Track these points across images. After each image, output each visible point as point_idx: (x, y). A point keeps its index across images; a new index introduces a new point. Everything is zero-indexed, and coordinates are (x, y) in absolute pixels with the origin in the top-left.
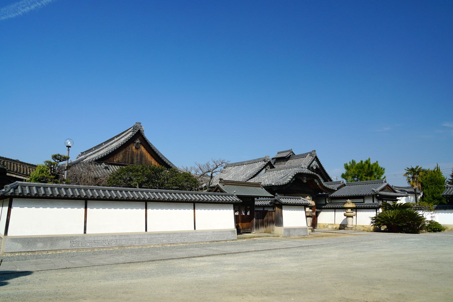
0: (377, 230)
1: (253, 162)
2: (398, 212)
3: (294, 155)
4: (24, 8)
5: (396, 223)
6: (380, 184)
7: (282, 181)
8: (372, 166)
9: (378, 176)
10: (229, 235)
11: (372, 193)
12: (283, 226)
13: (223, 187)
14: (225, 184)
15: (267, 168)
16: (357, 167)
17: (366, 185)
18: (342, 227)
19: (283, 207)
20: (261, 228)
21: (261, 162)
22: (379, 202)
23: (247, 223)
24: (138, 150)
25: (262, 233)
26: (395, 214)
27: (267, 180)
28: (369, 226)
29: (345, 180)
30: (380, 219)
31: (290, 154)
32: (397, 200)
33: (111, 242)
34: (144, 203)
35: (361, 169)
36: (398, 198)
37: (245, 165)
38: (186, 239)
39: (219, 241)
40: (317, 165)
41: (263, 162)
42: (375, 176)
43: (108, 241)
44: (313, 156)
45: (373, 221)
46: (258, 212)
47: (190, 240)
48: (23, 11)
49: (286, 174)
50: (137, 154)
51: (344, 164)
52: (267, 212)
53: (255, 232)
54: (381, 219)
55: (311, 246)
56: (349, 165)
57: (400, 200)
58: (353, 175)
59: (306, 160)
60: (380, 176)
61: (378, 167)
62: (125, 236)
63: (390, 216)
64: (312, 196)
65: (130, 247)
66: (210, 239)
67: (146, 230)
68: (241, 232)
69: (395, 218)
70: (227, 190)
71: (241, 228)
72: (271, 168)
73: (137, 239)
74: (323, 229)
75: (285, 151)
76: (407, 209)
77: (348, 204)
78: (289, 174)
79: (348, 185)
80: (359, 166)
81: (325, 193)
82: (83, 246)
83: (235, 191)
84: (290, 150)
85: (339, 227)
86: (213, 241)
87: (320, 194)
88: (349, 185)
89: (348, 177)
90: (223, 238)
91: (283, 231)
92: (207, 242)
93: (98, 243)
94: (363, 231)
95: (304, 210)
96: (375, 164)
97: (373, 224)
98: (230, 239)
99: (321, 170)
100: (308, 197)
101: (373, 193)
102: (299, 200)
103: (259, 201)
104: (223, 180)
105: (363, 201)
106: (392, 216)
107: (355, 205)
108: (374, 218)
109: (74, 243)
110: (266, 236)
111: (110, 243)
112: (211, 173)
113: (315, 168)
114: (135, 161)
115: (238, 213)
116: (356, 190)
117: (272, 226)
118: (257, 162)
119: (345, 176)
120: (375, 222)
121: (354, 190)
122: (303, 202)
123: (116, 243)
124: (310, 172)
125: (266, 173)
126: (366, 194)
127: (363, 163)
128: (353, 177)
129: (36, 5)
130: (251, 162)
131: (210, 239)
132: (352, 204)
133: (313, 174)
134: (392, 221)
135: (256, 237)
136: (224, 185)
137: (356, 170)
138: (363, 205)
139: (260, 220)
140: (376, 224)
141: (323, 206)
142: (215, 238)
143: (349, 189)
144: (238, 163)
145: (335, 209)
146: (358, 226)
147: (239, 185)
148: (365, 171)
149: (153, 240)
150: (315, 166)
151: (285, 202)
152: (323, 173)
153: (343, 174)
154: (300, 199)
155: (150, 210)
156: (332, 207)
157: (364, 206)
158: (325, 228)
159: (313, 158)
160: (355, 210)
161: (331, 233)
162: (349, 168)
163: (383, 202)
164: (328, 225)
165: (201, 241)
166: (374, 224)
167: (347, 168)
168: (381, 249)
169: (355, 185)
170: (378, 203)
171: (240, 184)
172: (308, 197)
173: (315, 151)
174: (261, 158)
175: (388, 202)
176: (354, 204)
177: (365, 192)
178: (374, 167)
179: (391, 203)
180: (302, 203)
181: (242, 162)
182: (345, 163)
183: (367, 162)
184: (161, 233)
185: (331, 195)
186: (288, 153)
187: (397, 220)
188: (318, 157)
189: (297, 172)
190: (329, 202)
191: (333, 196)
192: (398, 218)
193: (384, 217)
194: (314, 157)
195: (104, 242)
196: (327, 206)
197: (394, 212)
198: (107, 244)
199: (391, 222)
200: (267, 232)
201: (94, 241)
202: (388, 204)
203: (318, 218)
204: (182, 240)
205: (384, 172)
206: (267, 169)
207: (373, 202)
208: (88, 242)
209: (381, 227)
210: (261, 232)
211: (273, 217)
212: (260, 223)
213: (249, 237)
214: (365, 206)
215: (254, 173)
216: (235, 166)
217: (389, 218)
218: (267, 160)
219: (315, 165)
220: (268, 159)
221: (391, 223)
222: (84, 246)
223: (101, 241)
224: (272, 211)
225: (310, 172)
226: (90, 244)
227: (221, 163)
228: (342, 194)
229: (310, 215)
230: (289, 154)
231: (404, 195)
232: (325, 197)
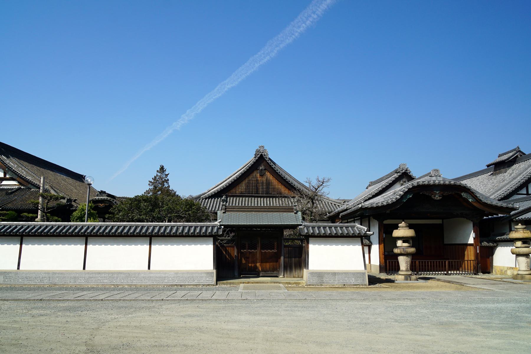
3: (523, 156)
4: (299, 27)
10: (202, 278)
12: (308, 268)
19: (311, 240)
23: (271, 263)
24: (263, 178)
33: (43, 280)
34: (148, 238)
38: (135, 280)
39: (185, 285)
43: (40, 278)
47: (140, 282)
48: (299, 31)
50: (263, 182)
62: (59, 273)
64: (472, 221)
65: (160, 286)
67: (84, 268)
68: (261, 275)
71: (260, 269)
73: (72, 278)
82: (15, 282)
90: (191, 282)
93: (30, 280)
95: (149, 244)
98: (203, 283)
100: (520, 224)
109: (7, 278)
111: (42, 281)
114: (260, 191)
123: (48, 281)
129: (311, 19)
131: (171, 282)
139: (293, 259)
141: (497, 238)
149: (91, 280)
155: (91, 246)
164: (506, 269)
165: (156, 284)
184: (103, 272)
195: (37, 279)
198: (40, 281)
201: (26, 278)
204: (130, 282)
208: (20, 278)
222: (16, 281)
223: (33, 278)
226: (22, 280)
229: (403, 252)
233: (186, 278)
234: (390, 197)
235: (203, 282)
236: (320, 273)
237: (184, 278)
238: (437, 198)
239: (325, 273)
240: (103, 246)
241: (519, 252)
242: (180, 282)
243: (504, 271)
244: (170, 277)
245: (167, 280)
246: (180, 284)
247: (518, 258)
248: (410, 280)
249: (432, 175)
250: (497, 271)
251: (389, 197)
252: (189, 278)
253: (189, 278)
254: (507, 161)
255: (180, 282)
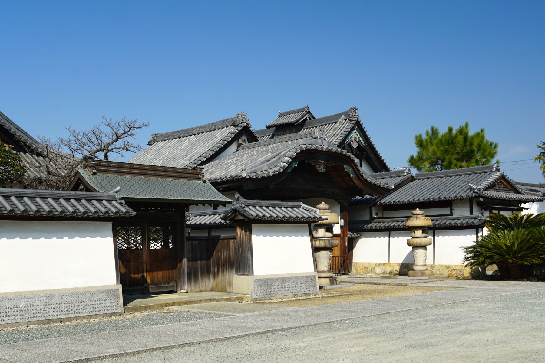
0: (479, 276)
1: (210, 130)
2: (523, 235)
5: (518, 258)
6: (487, 174)
7: (266, 168)
8: (472, 138)
9: (484, 160)
10: (98, 302)
11: (469, 194)
13: (91, 179)
14: (98, 170)
15: (240, 142)
16: (441, 141)
17: (456, 178)
18: (405, 270)
19: (254, 226)
20: (202, 277)
21: (228, 128)
22: (482, 213)
25: (206, 291)
26: (517, 239)
27: (233, 167)
28: (460, 266)
29: (417, 169)
30: (483, 250)
31: (304, 116)
32: (521, 209)
35: (448, 145)
36: (523, 205)
37: (194, 135)
39: (70, 320)
40: (361, 139)
41: (232, 126)
42: (477, 161)
44: (351, 121)
45: (468, 256)
46: (195, 240)
49: (277, 153)
51: (414, 137)
52: (218, 241)
53: (185, 291)
54: (486, 251)
55: (298, 327)
56: (424, 137)
57: (527, 209)
58: (432, 159)
59: (336, 128)
60: (488, 161)
61: (485, 140)
63: (505, 244)
64: (339, 203)
66: (38, 315)
69: (516, 247)
70: (105, 188)
72: (249, 142)
74: (364, 276)
75: (294, 111)
76: (542, 228)
77: (417, 218)
78: (284, 151)
79: (419, 179)
80: (445, 139)
81: (368, 197)
83: (119, 188)
84: (304, 108)
85: (398, 270)
86: (50, 321)
87: (359, 198)
88: (420, 177)
89: (423, 163)
90: (80, 311)
91: (252, 284)
92: (28, 324)
94: (449, 277)
96: (478, 135)
97: (468, 262)
99: (369, 151)
100: (418, 209)
101: (470, 194)
102: (297, 210)
103: (208, 216)
104: (94, 161)
105: (449, 213)
106: (509, 244)
107: (432, 220)
108: (470, 249)
110: (206, 300)
112: (103, 153)
113: (355, 145)
115: (158, 245)
116: (436, 189)
117: (228, 275)
118: (218, 129)
119: (417, 162)
120: (473, 258)
121: (431, 189)
122: (305, 216)
124: (332, 149)
125: (238, 152)
126: (455, 197)
127: (454, 132)
128: (433, 164)
130: (206, 130)
131: (40, 315)
132: (423, 218)
133: (341, 153)
134: (509, 256)
135: (180, 305)
136: (94, 174)
137: (438, 147)
138: (448, 220)
139: (199, 262)
140: (475, 262)
142: (55, 314)
143: (422, 187)
144: (179, 132)
145: (389, 231)
146: (437, 268)
147: (140, 174)
148: (458, 149)
150: (355, 143)
151: (257, 215)
152: (371, 156)
153: (412, 157)
154: (298, 208)
156: (382, 226)
157: (450, 223)
158: (368, 273)
159: (351, 125)
160: (432, 231)
161: (375, 284)
162: (424, 144)
163: (491, 212)
165: (9, 322)
166: (471, 261)
167: (420, 143)
168: (479, 331)
169: (435, 179)
170: (480, 215)
171: (143, 172)
172: (323, 205)
173: (355, 109)
174: (227, 120)
175: (502, 213)
176: (428, 218)
177: (454, 191)
178: (476, 142)
179: (507, 214)
180: (300, 216)
181: (188, 130)
182: (418, 134)
183: (461, 131)
185: (383, 201)
186: (300, 115)
187: (520, 252)
188: (361, 123)
189: (302, 147)
190: (378, 216)
191: (387, 202)
192: (522, 247)
193: (492, 245)
194: (353, 122)
196: (373, 225)
197: (513, 236)
199: (507, 256)
200: (218, 289)
202: (501, 217)
203: (355, 251)
205: (495, 153)
206: (241, 144)
207: (471, 213)
209: (485, 267)
210: (204, 289)
211: (231, 253)
212: (201, 268)
213: (158, 305)
214: (453, 223)
215: (209, 152)
216: (172, 139)
217: (503, 248)
218: (242, 123)
219: (355, 139)
220: (242, 120)
221: (508, 259)
224: (229, 239)
225: (332, 149)
227: (129, 129)
228: (406, 197)
229: (328, 245)
230: (303, 118)
231: (536, 197)
232: (370, 204)
233: (70, 305)
234: (275, 164)
235: (101, 309)
236: (267, 279)
237: (66, 305)
238: (321, 169)
239: (273, 279)
240: (78, 239)
241: (420, 243)
242: (58, 313)
243: (370, 269)
244: (38, 305)
245: (33, 312)
246: (59, 317)
247: (416, 250)
248: (336, 284)
249: (317, 136)
250: (359, 270)
251: (274, 164)
252: (76, 304)
253: (76, 304)
254: (297, 123)
255: (58, 313)
